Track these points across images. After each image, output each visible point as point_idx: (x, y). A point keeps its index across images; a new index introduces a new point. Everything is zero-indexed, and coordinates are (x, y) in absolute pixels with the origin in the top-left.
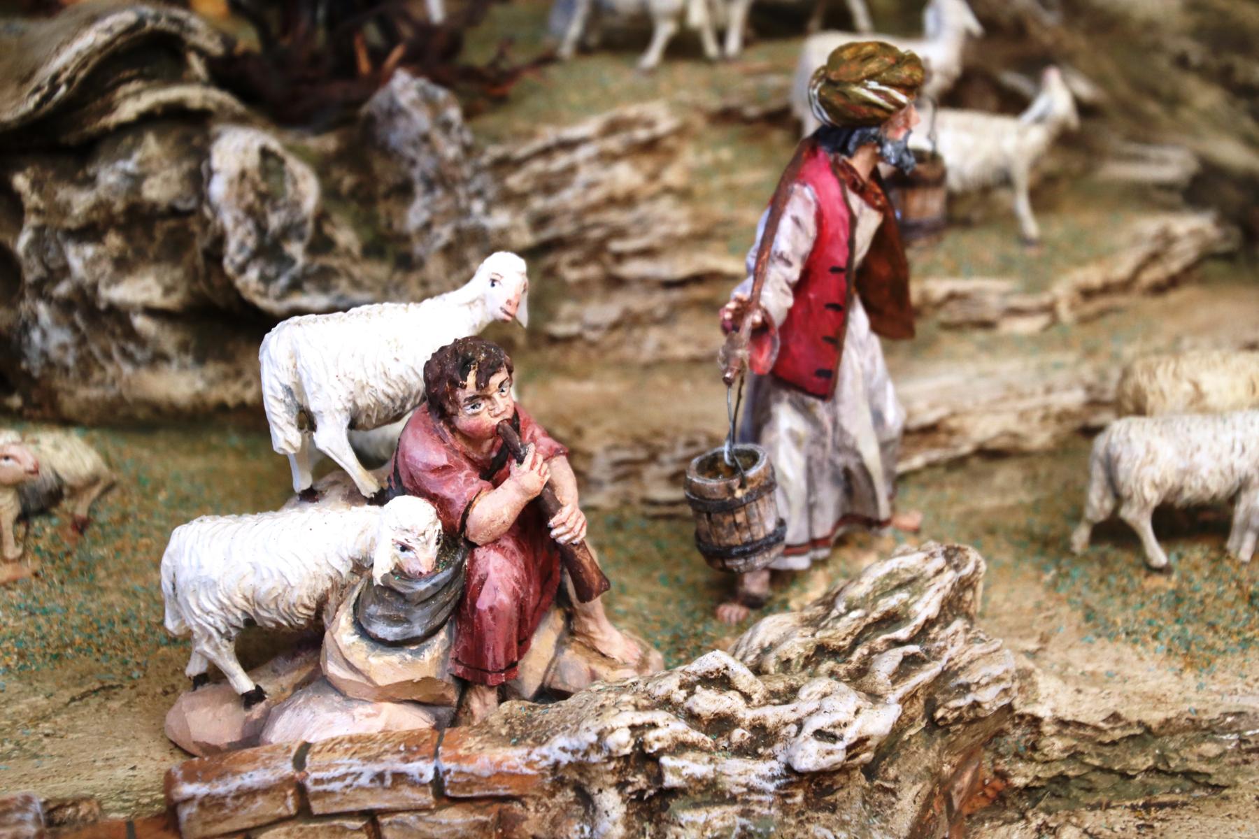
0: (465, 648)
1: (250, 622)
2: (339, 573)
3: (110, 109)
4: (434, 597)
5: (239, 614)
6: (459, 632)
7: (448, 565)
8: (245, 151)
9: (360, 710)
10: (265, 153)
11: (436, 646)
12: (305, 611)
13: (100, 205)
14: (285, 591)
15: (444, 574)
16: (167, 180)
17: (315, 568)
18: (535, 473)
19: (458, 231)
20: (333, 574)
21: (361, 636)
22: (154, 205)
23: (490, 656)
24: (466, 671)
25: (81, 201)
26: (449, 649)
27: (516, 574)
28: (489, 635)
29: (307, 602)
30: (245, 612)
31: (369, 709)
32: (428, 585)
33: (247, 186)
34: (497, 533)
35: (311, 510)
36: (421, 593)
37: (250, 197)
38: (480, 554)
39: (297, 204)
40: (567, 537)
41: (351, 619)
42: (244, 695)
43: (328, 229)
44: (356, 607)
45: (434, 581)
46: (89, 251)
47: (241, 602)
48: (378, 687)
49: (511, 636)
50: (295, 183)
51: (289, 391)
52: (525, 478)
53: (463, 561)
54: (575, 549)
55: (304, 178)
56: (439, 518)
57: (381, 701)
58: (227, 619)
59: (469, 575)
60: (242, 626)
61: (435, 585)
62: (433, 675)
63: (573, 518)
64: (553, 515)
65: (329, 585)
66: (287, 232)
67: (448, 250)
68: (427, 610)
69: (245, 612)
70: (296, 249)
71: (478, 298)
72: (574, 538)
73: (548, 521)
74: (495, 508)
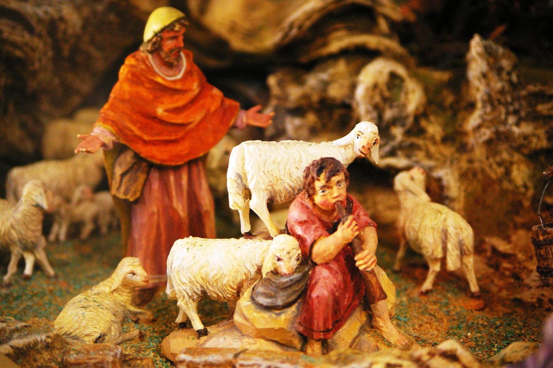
0: (305, 317)
1: (204, 292)
2: (250, 272)
3: (325, 44)
4: (290, 286)
5: (199, 286)
6: (303, 308)
7: (299, 272)
8: (381, 72)
9: (246, 340)
10: (393, 76)
11: (289, 313)
12: (231, 290)
13: (306, 97)
14: (221, 277)
15: (296, 276)
16: (342, 86)
17: (238, 267)
18: (349, 230)
19: (497, 133)
20: (246, 272)
21: (253, 303)
22: (333, 100)
23: (316, 322)
24: (304, 330)
25: (295, 93)
26: (296, 316)
27: (335, 282)
28: (316, 311)
29: (232, 284)
30: (202, 286)
31: (251, 341)
32: (288, 279)
33: (377, 92)
34: (327, 259)
35: (249, 241)
36: (284, 283)
37: (377, 99)
38: (318, 269)
39: (404, 106)
40: (364, 266)
41: (250, 294)
42: (198, 331)
43: (423, 123)
44: (253, 289)
45: (291, 278)
46: (297, 121)
47: (200, 280)
48: (256, 329)
49: (328, 314)
50: (407, 93)
51: (239, 176)
52: (344, 232)
53: (309, 271)
54: (368, 274)
55: (414, 91)
56: (300, 248)
57: (258, 338)
58: (192, 288)
59: (311, 278)
60: (200, 293)
61: (291, 280)
62: (285, 327)
63: (368, 257)
64: (358, 254)
65: (244, 277)
66: (395, 121)
67: (489, 143)
68: (286, 293)
69: (202, 286)
70: (398, 132)
71: (350, 144)
72: (368, 267)
73: (354, 256)
74: (327, 246)
